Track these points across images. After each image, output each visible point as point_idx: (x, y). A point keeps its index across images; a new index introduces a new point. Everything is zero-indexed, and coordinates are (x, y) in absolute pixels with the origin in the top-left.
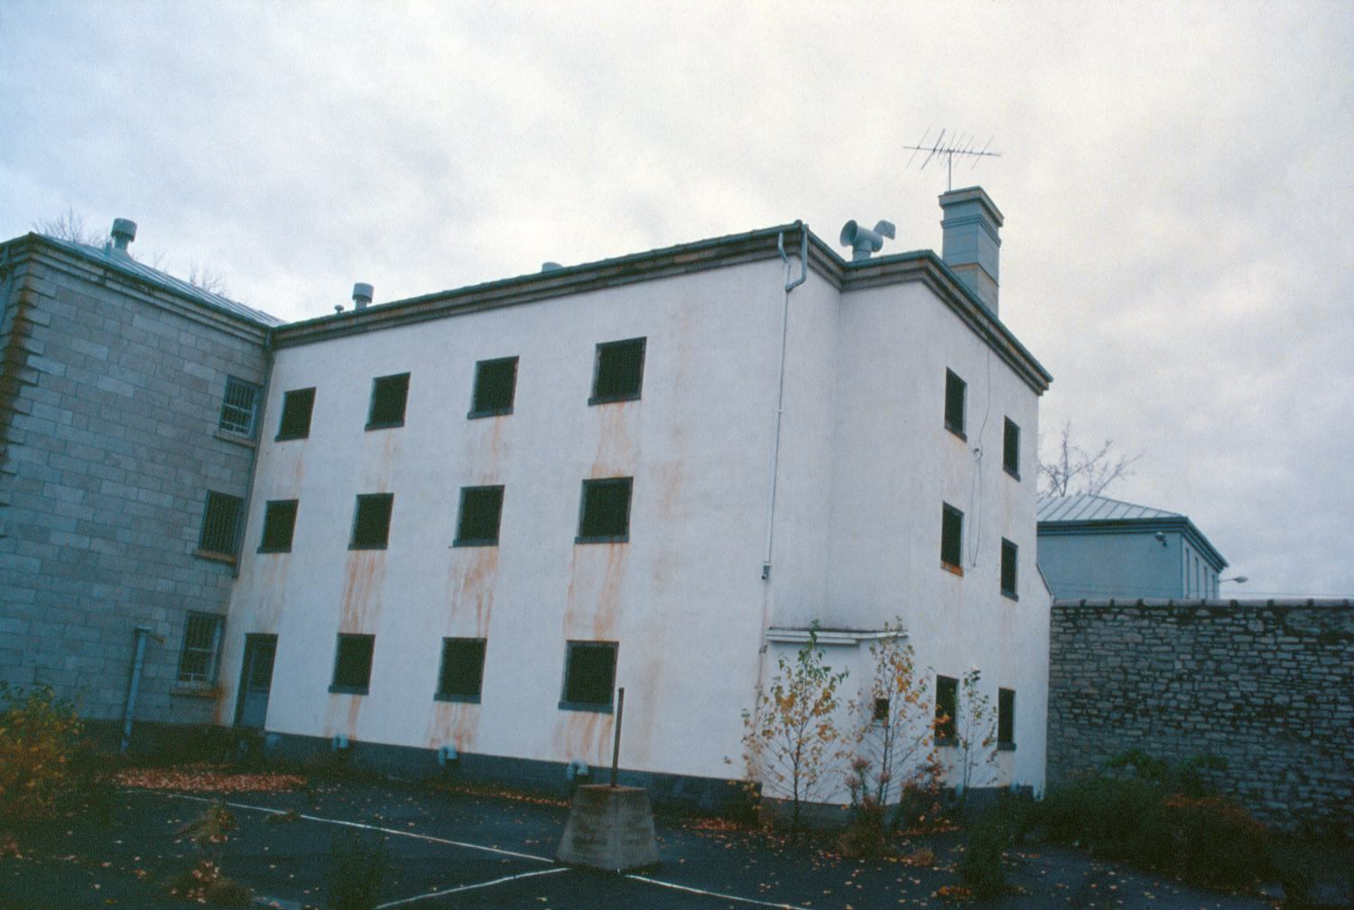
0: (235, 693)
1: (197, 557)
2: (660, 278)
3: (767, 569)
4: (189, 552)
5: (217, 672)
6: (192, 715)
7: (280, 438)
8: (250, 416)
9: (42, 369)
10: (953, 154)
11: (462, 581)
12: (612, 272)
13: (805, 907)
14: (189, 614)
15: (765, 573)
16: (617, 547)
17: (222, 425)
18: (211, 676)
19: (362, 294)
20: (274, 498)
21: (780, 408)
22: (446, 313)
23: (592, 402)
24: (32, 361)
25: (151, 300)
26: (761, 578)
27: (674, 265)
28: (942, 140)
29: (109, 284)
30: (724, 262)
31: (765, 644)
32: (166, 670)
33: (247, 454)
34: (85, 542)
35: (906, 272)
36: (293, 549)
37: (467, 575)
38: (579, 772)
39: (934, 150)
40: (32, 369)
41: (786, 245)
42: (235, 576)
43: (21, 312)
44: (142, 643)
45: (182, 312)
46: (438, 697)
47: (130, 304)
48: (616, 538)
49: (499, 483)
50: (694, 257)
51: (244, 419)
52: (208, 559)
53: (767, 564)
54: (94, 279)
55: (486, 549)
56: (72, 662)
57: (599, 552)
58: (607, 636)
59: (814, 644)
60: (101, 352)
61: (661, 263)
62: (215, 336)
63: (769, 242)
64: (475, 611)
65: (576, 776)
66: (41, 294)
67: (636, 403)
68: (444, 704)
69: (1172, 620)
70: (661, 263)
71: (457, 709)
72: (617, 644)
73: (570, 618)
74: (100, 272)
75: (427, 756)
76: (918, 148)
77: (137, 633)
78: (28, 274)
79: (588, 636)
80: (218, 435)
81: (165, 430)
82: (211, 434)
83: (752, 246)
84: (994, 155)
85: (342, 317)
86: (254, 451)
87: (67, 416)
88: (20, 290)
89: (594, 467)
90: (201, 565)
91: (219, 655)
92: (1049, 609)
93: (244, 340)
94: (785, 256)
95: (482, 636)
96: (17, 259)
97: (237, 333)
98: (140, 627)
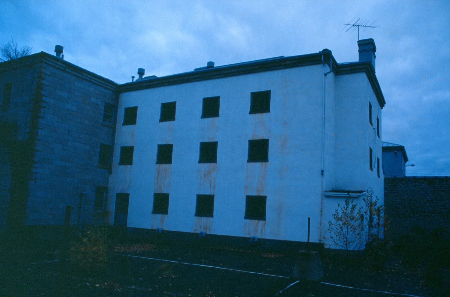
0: (114, 214)
3: (322, 171)
7: (124, 124)
11: (203, 175)
13: (420, 296)
15: (322, 173)
16: (264, 163)
19: (141, 72)
20: (123, 145)
21: (324, 116)
23: (251, 112)
24: (44, 98)
25: (80, 76)
38: (255, 240)
39: (353, 25)
41: (324, 59)
46: (196, 215)
49: (215, 141)
53: (323, 170)
54: (62, 68)
55: (212, 164)
57: (257, 166)
58: (262, 194)
59: (350, 197)
66: (46, 74)
67: (268, 114)
68: (198, 218)
69: (426, 183)
74: (64, 66)
76: (348, 24)
82: (100, 123)
86: (114, 129)
93: (110, 90)
95: (212, 194)
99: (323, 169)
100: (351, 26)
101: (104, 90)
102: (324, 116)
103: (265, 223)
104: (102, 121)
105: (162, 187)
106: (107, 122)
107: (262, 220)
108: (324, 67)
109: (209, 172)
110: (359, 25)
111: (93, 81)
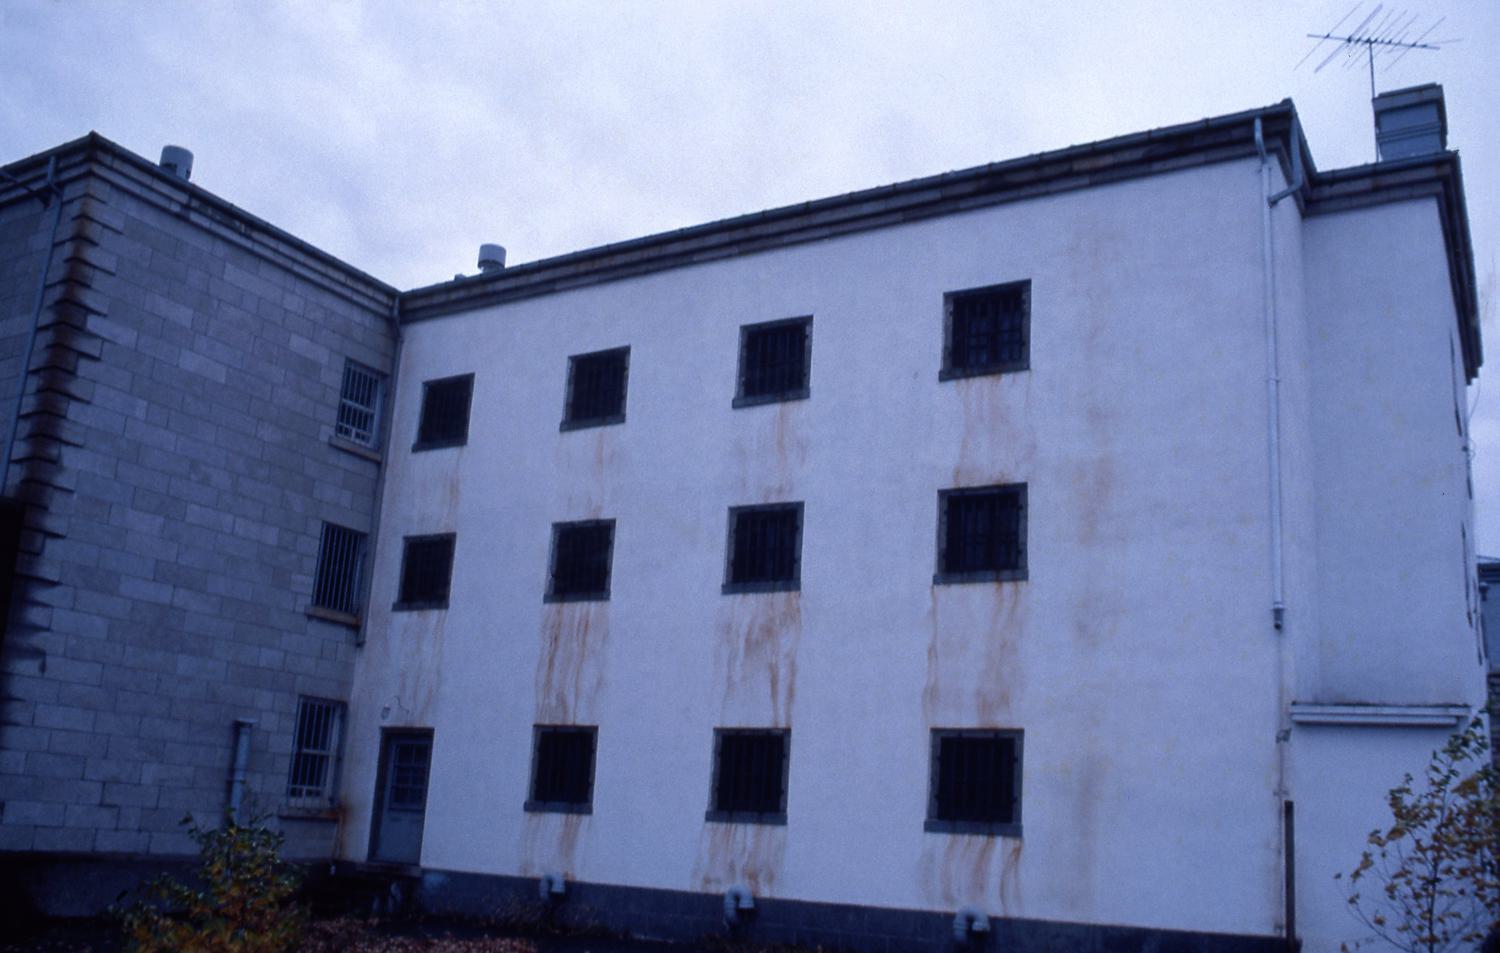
1: (310, 617)
2: (1048, 194)
3: (1278, 613)
4: (301, 609)
5: (337, 780)
6: (306, 846)
8: (372, 416)
9: (105, 335)
10: (1373, 45)
11: (742, 644)
12: (968, 188)
14: (301, 700)
16: (1008, 587)
17: (339, 429)
18: (328, 789)
22: (685, 260)
23: (945, 376)
24: (92, 323)
25: (248, 244)
26: (1273, 628)
27: (1070, 174)
28: (1367, 27)
29: (194, 217)
30: (1157, 166)
31: (1286, 727)
32: (272, 783)
33: (370, 470)
34: (165, 594)
35: (1411, 184)
36: (451, 602)
37: (749, 633)
39: (1349, 40)
40: (94, 336)
41: (1266, 136)
42: (360, 645)
43: (77, 250)
44: (244, 740)
45: (288, 264)
46: (711, 817)
47: (221, 249)
48: (1006, 574)
50: (1108, 160)
51: (363, 421)
52: (322, 620)
53: (1281, 606)
54: (175, 208)
55: (780, 597)
56: (150, 773)
57: (977, 597)
58: (1002, 720)
60: (183, 315)
61: (1048, 171)
62: (328, 301)
63: (1237, 133)
64: (767, 689)
65: (970, 932)
66: (105, 226)
67: (1022, 376)
68: (722, 827)
70: (1048, 171)
71: (745, 834)
72: (1020, 732)
73: (932, 694)
74: (183, 198)
75: (706, 904)
76: (1328, 36)
77: (238, 727)
78: (87, 195)
79: (967, 720)
80: (335, 442)
81: (267, 433)
83: (1209, 140)
84: (1431, 48)
85: (461, 283)
87: (141, 409)
88: (74, 219)
89: (957, 472)
90: (315, 629)
91: (339, 759)
92: (1484, 680)
94: (1265, 154)
95: (782, 725)
96: (66, 176)
97: (356, 298)
98: (241, 719)
99: (1281, 603)
100: (1342, 42)
101: (341, 308)
102: (1273, 376)
103: (1017, 851)
104: (332, 432)
105: (571, 700)
106: (350, 436)
107: (1005, 835)
108: (1265, 171)
109: (769, 631)
110: (1373, 39)
111: (297, 268)
